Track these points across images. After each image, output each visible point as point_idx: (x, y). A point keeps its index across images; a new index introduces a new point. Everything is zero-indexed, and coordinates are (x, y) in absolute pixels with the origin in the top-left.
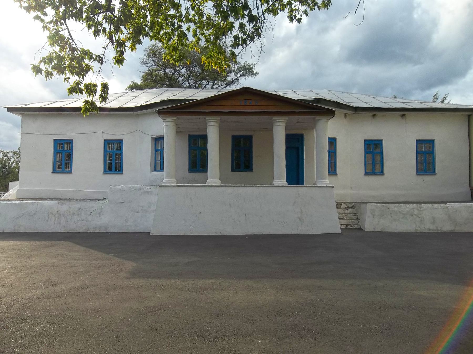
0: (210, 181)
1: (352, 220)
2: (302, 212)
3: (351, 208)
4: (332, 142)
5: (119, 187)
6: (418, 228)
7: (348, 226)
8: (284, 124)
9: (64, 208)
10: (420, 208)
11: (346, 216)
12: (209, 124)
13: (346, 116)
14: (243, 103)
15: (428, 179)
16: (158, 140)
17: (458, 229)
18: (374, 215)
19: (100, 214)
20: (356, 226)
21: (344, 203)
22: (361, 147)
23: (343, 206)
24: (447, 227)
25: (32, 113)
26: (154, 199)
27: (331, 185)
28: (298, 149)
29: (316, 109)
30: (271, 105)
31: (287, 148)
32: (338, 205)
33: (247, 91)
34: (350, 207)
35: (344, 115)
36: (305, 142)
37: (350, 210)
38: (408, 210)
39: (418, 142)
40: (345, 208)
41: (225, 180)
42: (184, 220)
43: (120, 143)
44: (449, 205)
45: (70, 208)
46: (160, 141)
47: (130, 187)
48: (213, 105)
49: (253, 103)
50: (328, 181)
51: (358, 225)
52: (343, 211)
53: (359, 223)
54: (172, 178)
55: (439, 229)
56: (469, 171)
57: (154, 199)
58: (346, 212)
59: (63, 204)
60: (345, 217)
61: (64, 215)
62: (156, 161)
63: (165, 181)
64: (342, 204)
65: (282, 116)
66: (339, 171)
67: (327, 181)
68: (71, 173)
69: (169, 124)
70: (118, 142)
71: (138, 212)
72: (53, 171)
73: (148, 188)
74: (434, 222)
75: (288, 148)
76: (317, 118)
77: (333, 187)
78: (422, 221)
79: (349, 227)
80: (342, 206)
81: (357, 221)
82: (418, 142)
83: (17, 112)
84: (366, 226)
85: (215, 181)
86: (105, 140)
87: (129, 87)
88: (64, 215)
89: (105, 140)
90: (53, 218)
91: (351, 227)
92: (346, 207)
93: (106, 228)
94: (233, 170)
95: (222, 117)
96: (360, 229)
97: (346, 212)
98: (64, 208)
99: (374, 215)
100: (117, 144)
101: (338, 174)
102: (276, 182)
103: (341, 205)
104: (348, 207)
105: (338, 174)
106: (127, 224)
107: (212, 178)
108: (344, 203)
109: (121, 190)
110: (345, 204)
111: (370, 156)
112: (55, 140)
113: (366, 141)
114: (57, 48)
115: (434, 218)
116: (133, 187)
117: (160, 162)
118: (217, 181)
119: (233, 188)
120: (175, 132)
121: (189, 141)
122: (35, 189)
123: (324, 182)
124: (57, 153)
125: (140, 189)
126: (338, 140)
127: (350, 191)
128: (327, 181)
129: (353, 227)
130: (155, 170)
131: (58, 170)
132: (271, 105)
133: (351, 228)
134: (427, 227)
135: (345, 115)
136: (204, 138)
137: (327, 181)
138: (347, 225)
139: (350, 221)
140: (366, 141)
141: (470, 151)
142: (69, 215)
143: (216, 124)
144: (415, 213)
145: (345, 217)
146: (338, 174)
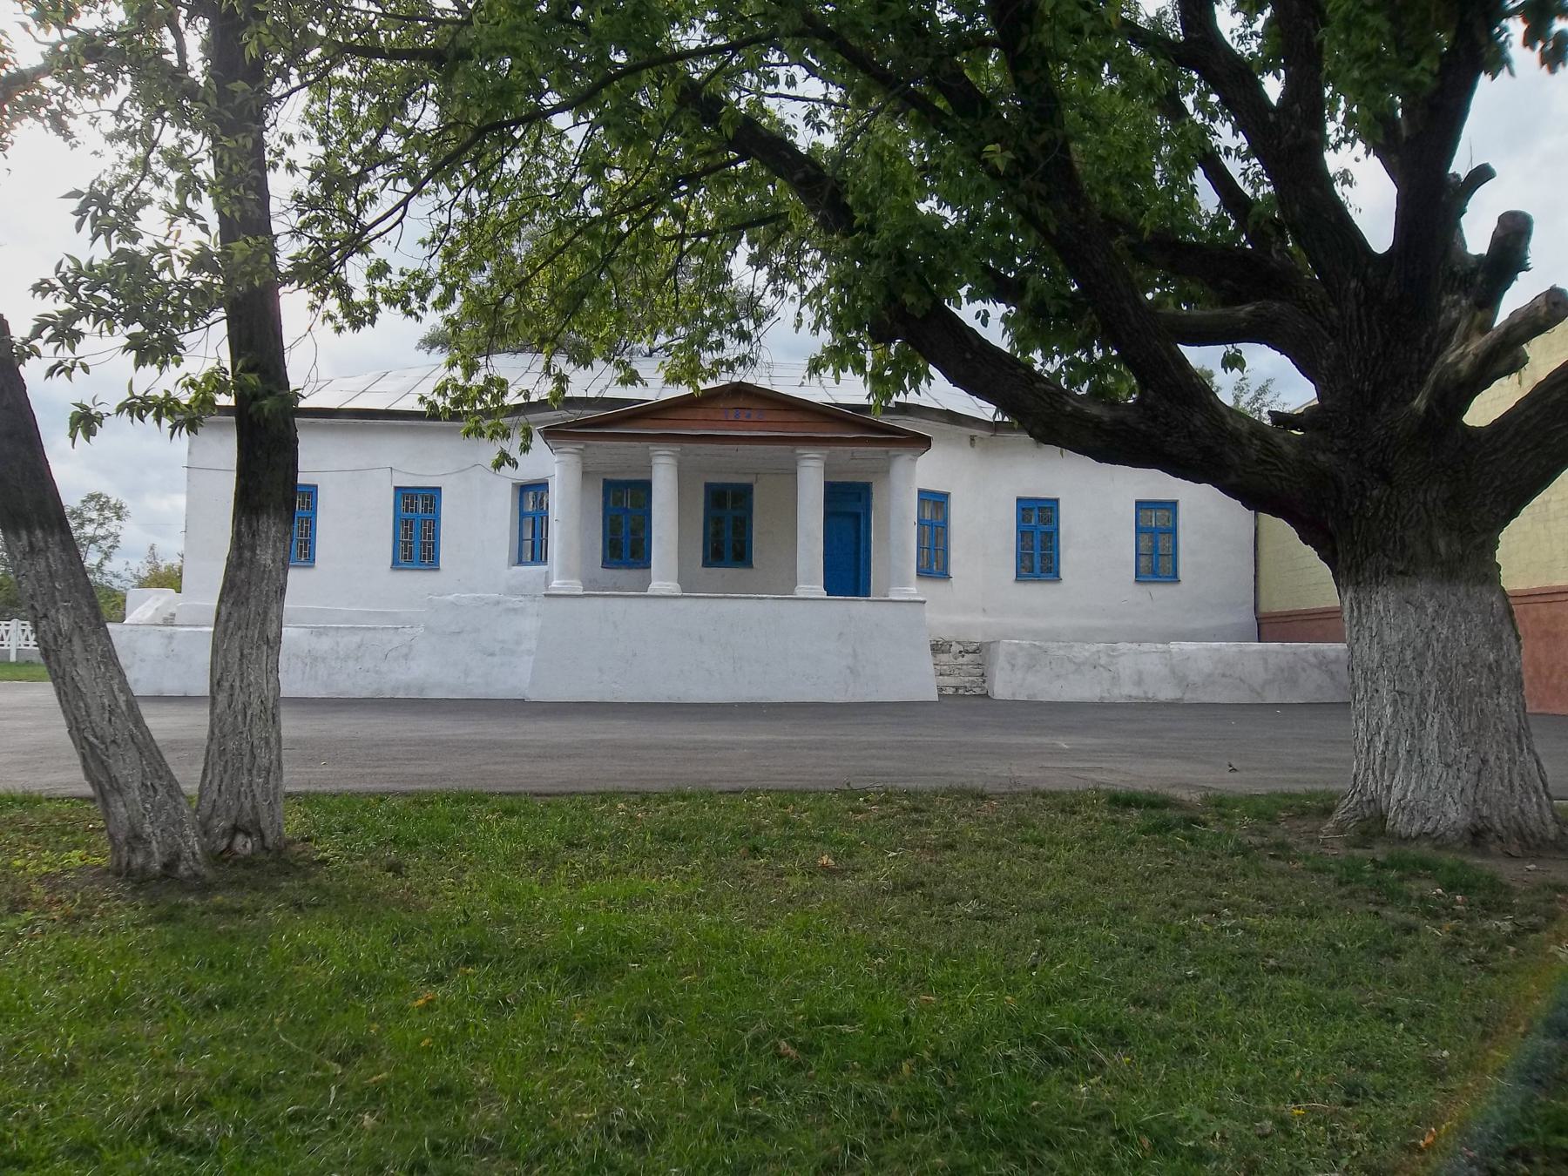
0: (656, 586)
2: (855, 656)
3: (974, 652)
4: (935, 503)
5: (450, 598)
6: (1106, 695)
8: (820, 464)
9: (324, 644)
10: (1113, 651)
14: (732, 415)
15: (1160, 591)
16: (532, 493)
17: (1189, 697)
18: (1013, 666)
19: (406, 657)
20: (978, 691)
21: (959, 643)
22: (1008, 518)
24: (1167, 693)
26: (529, 624)
27: (921, 599)
28: (857, 516)
29: (889, 433)
31: (828, 515)
32: (937, 648)
33: (741, 391)
36: (875, 501)
37: (968, 657)
38: (1087, 654)
39: (1140, 505)
41: (688, 586)
42: (600, 670)
43: (431, 496)
44: (1174, 646)
45: (338, 643)
46: (531, 493)
47: (474, 599)
49: (754, 416)
50: (914, 589)
51: (983, 688)
53: (986, 685)
54: (572, 578)
55: (1150, 696)
56: (1255, 577)
57: (529, 624)
58: (961, 660)
59: (321, 634)
60: (957, 672)
61: (324, 659)
62: (521, 540)
63: (556, 584)
67: (913, 589)
68: (313, 567)
69: (567, 458)
70: (428, 494)
71: (492, 655)
73: (515, 601)
74: (1139, 682)
75: (829, 515)
76: (893, 451)
77: (924, 602)
78: (1115, 680)
80: (953, 649)
82: (1140, 505)
84: (995, 689)
86: (396, 488)
87: (424, 341)
88: (324, 659)
89: (396, 488)
90: (300, 665)
93: (422, 690)
94: (706, 564)
95: (686, 445)
96: (986, 696)
97: (961, 660)
98: (324, 644)
99: (1013, 666)
100: (425, 498)
102: (802, 590)
106: (469, 680)
107: (660, 579)
108: (959, 643)
109: (454, 605)
111: (1145, 538)
113: (1019, 500)
114: (458, 372)
115: (1140, 673)
116: (482, 599)
117: (533, 543)
118: (672, 587)
119: (707, 601)
120: (579, 475)
121: (605, 494)
125: (498, 603)
126: (953, 497)
127: (981, 619)
130: (520, 562)
134: (1126, 691)
135: (972, 439)
136: (645, 487)
137: (913, 589)
138: (957, 689)
139: (966, 679)
140: (1019, 500)
141: (1256, 529)
142: (337, 658)
143: (670, 461)
144: (1102, 662)
145: (957, 672)
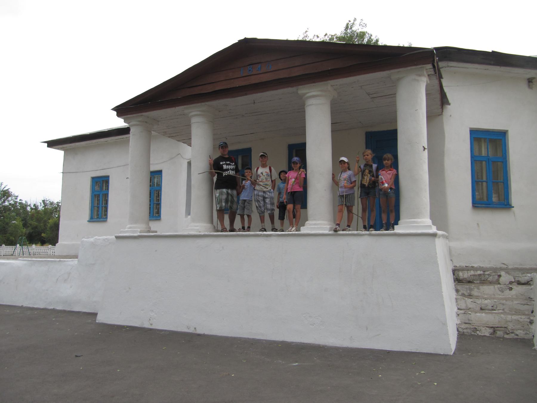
1: (515, 317)
7: (499, 330)
11: (503, 304)
12: (194, 120)
13: (531, 84)
20: (521, 333)
23: (505, 278)
25: (70, 146)
30: (281, 59)
34: (523, 282)
35: (526, 82)
40: (511, 283)
47: (104, 240)
48: (205, 84)
52: (500, 293)
64: (503, 273)
65: (314, 82)
66: (515, 200)
72: (91, 219)
79: (499, 333)
80: (502, 280)
81: (529, 320)
83: (61, 146)
85: (197, 226)
91: (508, 334)
92: (513, 280)
101: (513, 207)
103: (500, 276)
104: (518, 281)
105: (513, 206)
110: (509, 274)
112: (93, 178)
122: (66, 243)
123: (414, 222)
124: (95, 195)
128: (424, 220)
129: (513, 335)
131: (96, 217)
132: (281, 59)
133: (506, 336)
138: (494, 329)
139: (509, 317)
146: (513, 207)
